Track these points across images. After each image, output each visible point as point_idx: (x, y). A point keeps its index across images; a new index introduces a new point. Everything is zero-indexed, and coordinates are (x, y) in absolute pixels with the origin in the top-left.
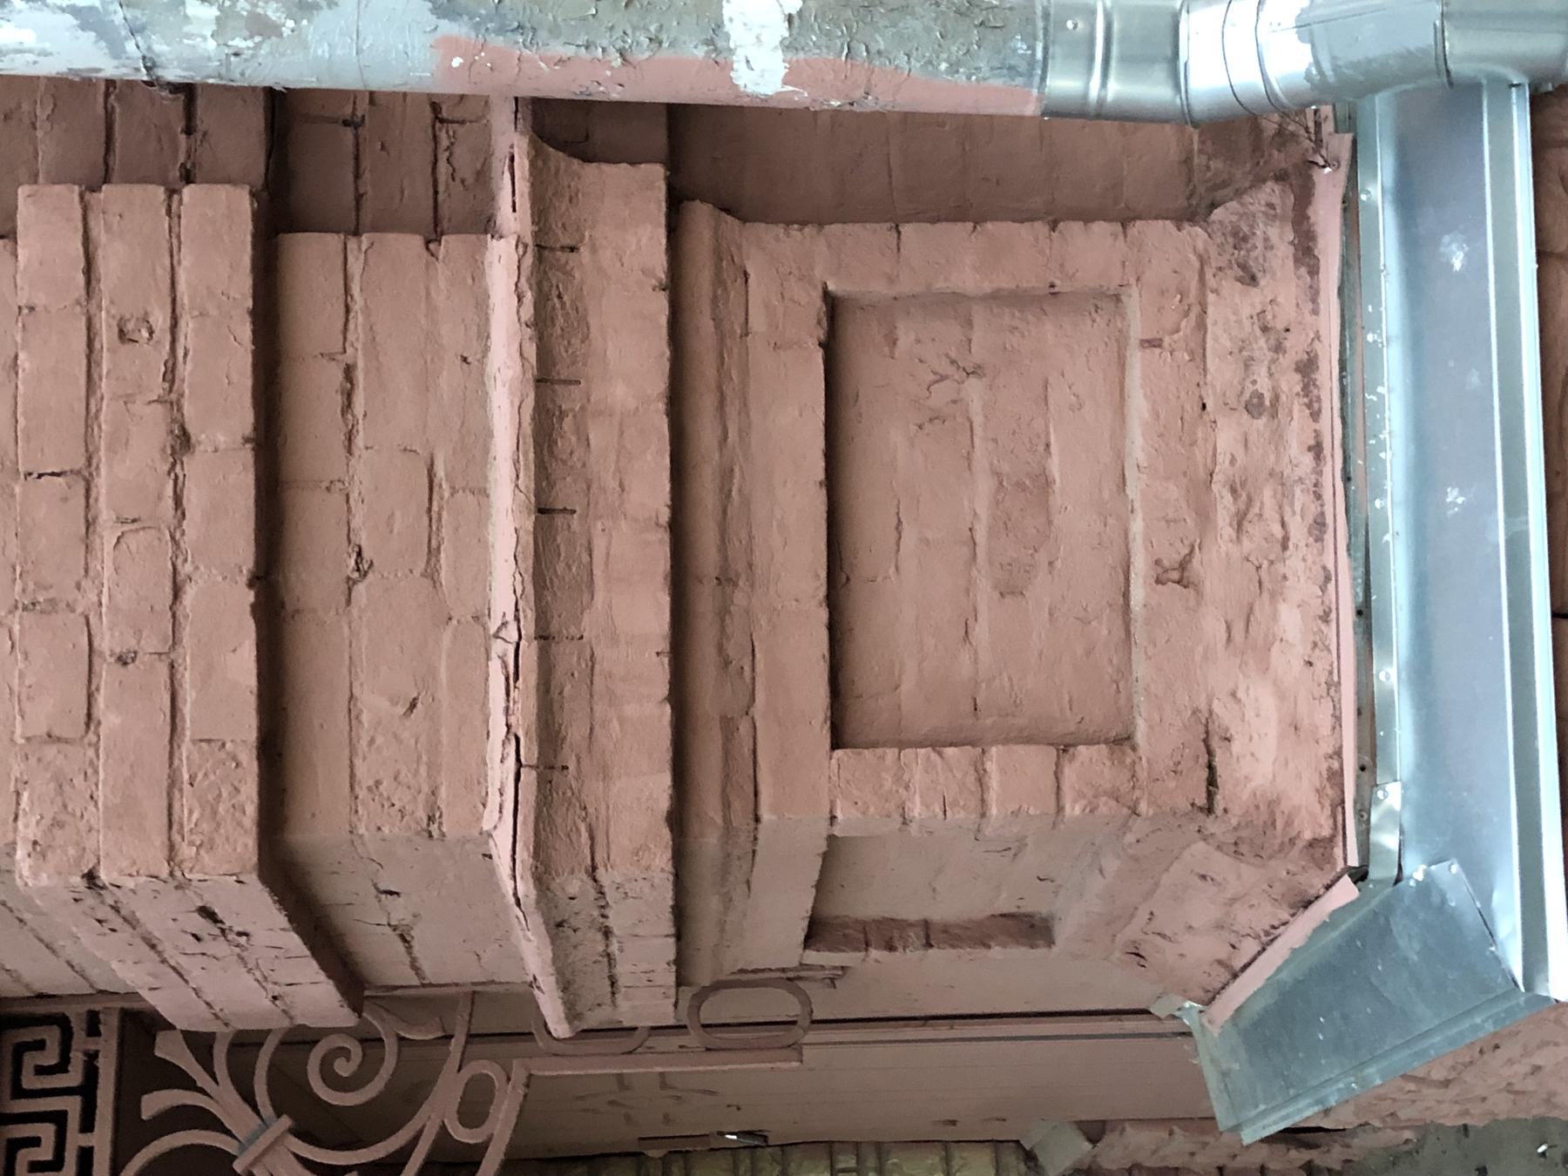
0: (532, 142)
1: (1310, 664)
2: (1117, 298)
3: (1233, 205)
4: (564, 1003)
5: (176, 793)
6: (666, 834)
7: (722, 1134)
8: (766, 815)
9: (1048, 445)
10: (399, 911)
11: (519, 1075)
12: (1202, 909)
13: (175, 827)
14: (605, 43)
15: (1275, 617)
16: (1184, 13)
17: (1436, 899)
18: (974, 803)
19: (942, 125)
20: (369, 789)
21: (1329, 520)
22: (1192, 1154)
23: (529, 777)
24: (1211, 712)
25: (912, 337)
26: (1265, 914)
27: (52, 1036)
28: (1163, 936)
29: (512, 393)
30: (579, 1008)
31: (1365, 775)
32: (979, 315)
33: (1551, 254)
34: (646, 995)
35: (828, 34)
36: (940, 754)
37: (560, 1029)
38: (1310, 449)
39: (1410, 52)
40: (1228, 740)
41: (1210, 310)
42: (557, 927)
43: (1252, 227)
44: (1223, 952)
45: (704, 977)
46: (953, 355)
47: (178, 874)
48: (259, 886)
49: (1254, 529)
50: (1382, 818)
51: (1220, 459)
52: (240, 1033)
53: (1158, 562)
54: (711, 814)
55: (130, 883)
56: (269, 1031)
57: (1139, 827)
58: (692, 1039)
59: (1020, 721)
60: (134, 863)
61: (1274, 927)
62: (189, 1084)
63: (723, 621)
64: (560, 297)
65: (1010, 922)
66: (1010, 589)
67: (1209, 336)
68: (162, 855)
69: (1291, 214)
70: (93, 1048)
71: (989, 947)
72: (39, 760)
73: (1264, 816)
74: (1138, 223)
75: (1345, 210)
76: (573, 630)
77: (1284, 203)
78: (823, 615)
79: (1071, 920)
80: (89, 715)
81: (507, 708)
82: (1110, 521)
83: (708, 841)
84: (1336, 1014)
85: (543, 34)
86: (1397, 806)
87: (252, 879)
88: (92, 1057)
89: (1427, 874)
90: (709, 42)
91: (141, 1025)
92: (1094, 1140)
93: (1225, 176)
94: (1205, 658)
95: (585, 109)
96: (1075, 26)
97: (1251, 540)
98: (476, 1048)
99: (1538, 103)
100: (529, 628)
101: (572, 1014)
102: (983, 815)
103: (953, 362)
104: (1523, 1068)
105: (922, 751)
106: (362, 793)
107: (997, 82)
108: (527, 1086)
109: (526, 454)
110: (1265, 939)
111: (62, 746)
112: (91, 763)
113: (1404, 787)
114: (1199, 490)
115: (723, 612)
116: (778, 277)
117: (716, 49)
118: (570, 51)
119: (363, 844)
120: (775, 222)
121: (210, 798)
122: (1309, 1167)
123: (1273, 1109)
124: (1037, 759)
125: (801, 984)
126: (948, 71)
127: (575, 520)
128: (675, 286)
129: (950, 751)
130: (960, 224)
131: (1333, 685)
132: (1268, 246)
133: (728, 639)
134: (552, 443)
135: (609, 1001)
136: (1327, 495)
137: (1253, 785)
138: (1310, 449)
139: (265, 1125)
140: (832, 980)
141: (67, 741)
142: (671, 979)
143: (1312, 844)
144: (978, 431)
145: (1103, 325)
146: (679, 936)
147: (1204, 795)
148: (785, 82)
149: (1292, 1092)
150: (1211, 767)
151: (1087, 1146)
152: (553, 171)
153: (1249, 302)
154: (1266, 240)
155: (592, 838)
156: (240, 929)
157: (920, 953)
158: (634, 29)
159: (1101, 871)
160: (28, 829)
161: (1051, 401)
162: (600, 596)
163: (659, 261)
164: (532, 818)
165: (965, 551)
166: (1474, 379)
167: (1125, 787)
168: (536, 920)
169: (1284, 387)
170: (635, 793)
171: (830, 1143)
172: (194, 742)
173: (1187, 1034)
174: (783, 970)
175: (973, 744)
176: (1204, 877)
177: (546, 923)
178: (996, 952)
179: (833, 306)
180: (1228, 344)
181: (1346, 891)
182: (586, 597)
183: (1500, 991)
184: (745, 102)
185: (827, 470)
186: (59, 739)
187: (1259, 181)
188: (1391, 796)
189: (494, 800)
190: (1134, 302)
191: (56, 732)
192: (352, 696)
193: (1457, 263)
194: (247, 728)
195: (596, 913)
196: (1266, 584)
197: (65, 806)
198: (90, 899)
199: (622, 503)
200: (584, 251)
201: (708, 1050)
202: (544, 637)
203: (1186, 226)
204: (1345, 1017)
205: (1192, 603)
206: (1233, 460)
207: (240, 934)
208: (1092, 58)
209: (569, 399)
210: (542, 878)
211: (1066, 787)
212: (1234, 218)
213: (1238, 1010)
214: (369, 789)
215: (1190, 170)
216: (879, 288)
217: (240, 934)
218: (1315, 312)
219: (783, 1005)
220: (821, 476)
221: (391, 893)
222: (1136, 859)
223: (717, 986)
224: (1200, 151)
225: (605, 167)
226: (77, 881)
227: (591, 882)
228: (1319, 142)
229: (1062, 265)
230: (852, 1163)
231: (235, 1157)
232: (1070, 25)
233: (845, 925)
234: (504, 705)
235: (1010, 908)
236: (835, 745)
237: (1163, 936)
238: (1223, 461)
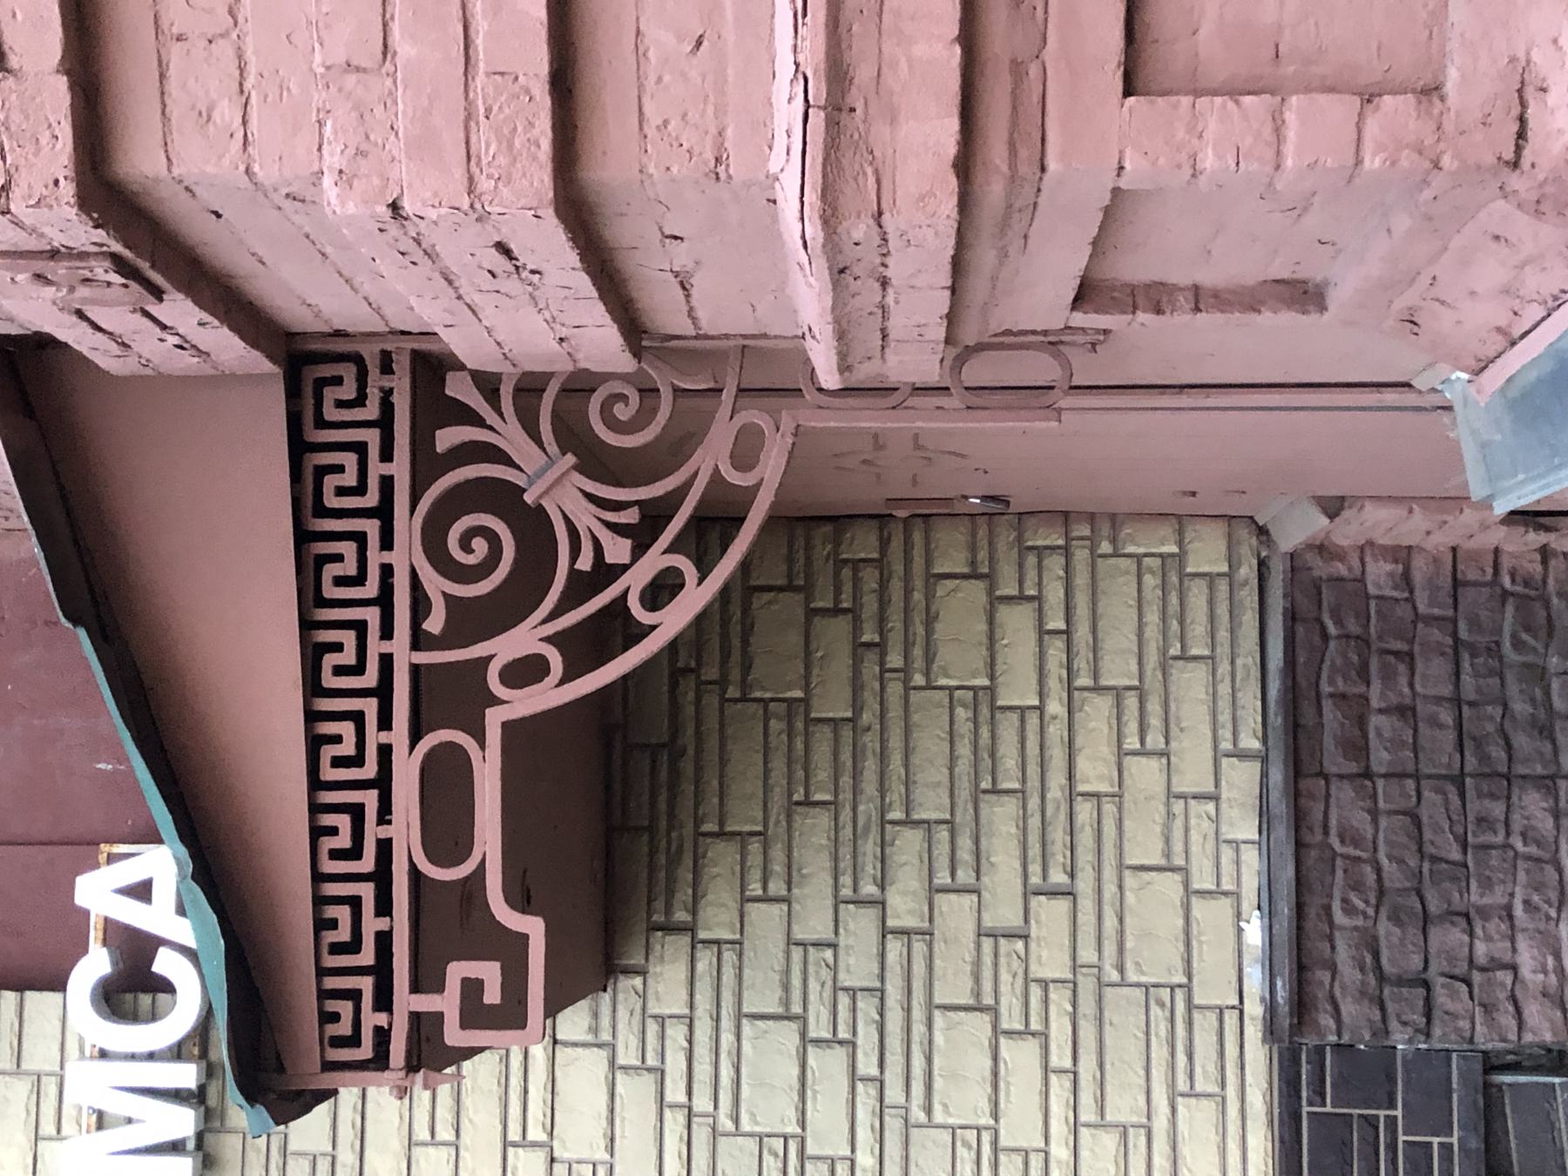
5: (473, 124)
6: (953, 182)
7: (966, 497)
8: (1053, 165)
10: (681, 256)
11: (787, 424)
13: (473, 163)
18: (1270, 154)
20: (658, 127)
22: (1428, 533)
23: (817, 119)
24: (1528, 62)
27: (348, 372)
28: (1443, 303)
36: (1237, 102)
37: (829, 379)
40: (1544, 90)
45: (969, 336)
47: (478, 206)
48: (555, 221)
52: (526, 375)
54: (998, 162)
55: (432, 214)
56: (552, 374)
57: (1438, 182)
58: (952, 402)
60: (436, 194)
62: (479, 422)
65: (1280, 287)
68: (462, 186)
70: (387, 385)
71: (1259, 312)
72: (340, 90)
80: (385, 46)
81: (795, 46)
83: (993, 190)
87: (549, 213)
88: (387, 394)
91: (432, 366)
92: (1332, 516)
98: (742, 402)
101: (844, 368)
102: (1278, 167)
105: (1218, 100)
106: (651, 131)
108: (795, 435)
110: (1551, 304)
111: (361, 75)
112: (390, 93)
119: (653, 184)
121: (506, 131)
123: (1533, 479)
124: (1341, 108)
125: (1061, 347)
129: (1247, 100)
135: (878, 354)
139: (551, 461)
140: (1094, 345)
141: (365, 70)
142: (941, 333)
146: (953, 290)
147: (1513, 148)
149: (1556, 461)
150: (1522, 120)
155: (878, 182)
156: (534, 267)
157: (1189, 317)
159: (1389, 230)
160: (333, 158)
164: (820, 160)
167: (1429, 141)
168: (821, 264)
171: (1066, 514)
172: (488, 74)
173: (1448, 408)
174: (1045, 333)
175: (1273, 93)
177: (830, 268)
178: (1267, 318)
186: (358, 69)
189: (780, 142)
191: (354, 63)
192: (638, 32)
194: (537, 61)
197: (367, 137)
198: (393, 229)
207: (533, 272)
210: (830, 219)
213: (1509, 380)
214: (658, 127)
217: (533, 272)
219: (1037, 368)
221: (676, 238)
223: (981, 347)
226: (383, 211)
227: (876, 228)
230: (1087, 532)
231: (524, 490)
233: (1113, 289)
234: (792, 42)
235: (1285, 274)
236: (1128, 92)
237: (1443, 303)
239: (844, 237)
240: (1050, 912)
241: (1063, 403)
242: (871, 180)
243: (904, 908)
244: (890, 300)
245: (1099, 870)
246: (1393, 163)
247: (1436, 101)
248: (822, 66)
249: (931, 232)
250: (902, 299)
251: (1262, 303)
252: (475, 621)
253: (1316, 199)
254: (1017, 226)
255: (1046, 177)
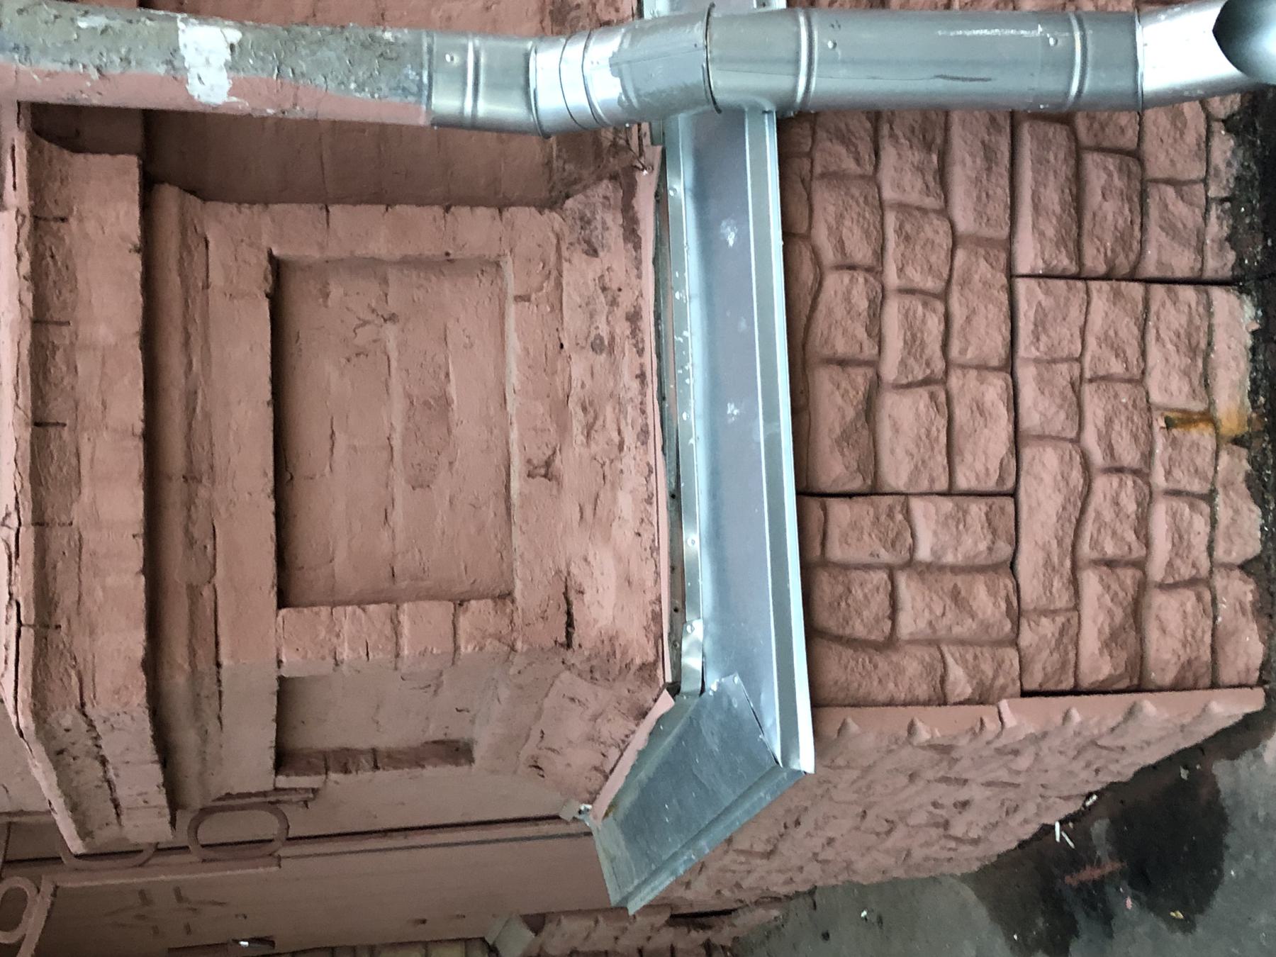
0: (30, 137)
1: (639, 535)
2: (498, 265)
3: (580, 197)
4: (75, 821)
7: (237, 942)
8: (225, 661)
9: (447, 375)
11: (47, 888)
12: (576, 726)
14: (86, 61)
15: (615, 500)
16: (533, 53)
17: (725, 703)
18: (391, 646)
19: (364, 131)
21: (651, 429)
22: (616, 938)
23: (28, 634)
24: (569, 573)
25: (341, 291)
26: (614, 727)
28: (553, 750)
29: (12, 331)
30: (89, 827)
31: (678, 615)
32: (393, 275)
33: (794, 235)
35: (263, 59)
36: (364, 610)
37: (76, 845)
38: (637, 377)
39: (687, 87)
41: (565, 273)
42: (58, 756)
43: (593, 213)
44: (597, 760)
46: (373, 305)
49: (598, 437)
50: (691, 645)
51: (574, 385)
53: (529, 461)
57: (518, 660)
59: (428, 583)
61: (627, 736)
63: (189, 510)
64: (52, 256)
66: (419, 483)
67: (565, 294)
69: (620, 203)
71: (423, 767)
73: (608, 648)
74: (512, 209)
75: (658, 202)
76: (64, 518)
77: (616, 198)
78: (271, 505)
79: (484, 739)
82: (496, 431)
83: (178, 682)
84: (674, 801)
85: (34, 54)
86: (701, 638)
89: (719, 685)
90: (169, 62)
92: (537, 930)
93: (576, 176)
94: (565, 531)
95: (75, 112)
96: (452, 59)
97: (597, 444)
99: (783, 126)
100: (27, 516)
101: (84, 833)
102: (397, 655)
103: (373, 311)
104: (818, 841)
105: (349, 609)
107: (397, 100)
109: (24, 380)
113: (705, 623)
114: (559, 410)
115: (189, 504)
116: (232, 246)
117: (174, 67)
118: (56, 67)
120: (230, 202)
122: (708, 946)
124: (439, 612)
125: (281, 807)
126: (356, 90)
127: (66, 433)
128: (148, 249)
129: (372, 608)
130: (375, 207)
131: (655, 550)
132: (605, 228)
133: (194, 524)
134: (46, 372)
136: (649, 410)
137: (599, 625)
138: (637, 377)
143: (643, 666)
144: (394, 364)
145: (488, 284)
148: (231, 93)
149: (653, 867)
150: (569, 614)
151: (530, 935)
152: (47, 159)
153: (593, 268)
154: (604, 223)
155: (81, 681)
158: (108, 51)
161: (449, 340)
162: (86, 491)
163: (133, 230)
164: (30, 667)
165: (385, 455)
166: (743, 325)
168: (39, 749)
169: (618, 331)
170: (116, 644)
175: (390, 602)
176: (573, 700)
178: (429, 771)
179: (278, 267)
180: (578, 300)
181: (666, 702)
182: (75, 491)
183: (768, 768)
184: (200, 108)
185: (273, 393)
187: (600, 179)
188: (696, 631)
190: (508, 268)
193: (731, 240)
195: (90, 743)
196: (609, 477)
199: (104, 417)
200: (73, 221)
201: (204, 861)
202: (40, 523)
203: (547, 211)
204: (680, 802)
205: (555, 492)
206: (583, 386)
208: (465, 84)
209: (61, 337)
210: (40, 711)
211: (461, 632)
212: (581, 207)
215: (551, 170)
216: (313, 254)
218: (639, 277)
219: (263, 825)
220: (269, 397)
222: (521, 687)
223: (206, 812)
224: (558, 156)
225: (90, 157)
228: (641, 152)
229: (454, 239)
232: (448, 58)
234: (7, 578)
235: (440, 736)
237: (553, 750)
238: (576, 384)
239: (55, 725)
241: (282, 852)
242: (75, 679)
244: (111, 774)
246: (481, 649)
247: (508, 602)
248: (31, 595)
249: (127, 719)
250: (121, 773)
251: (424, 759)
253: (444, 677)
254: (209, 709)
255: (222, 671)
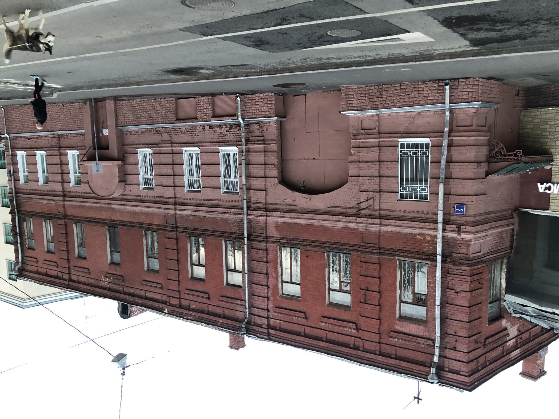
34: (488, 134)
116: (455, 128)
240: (549, 123)
243: (548, 134)
245: (81, 202)
252: (501, 155)
